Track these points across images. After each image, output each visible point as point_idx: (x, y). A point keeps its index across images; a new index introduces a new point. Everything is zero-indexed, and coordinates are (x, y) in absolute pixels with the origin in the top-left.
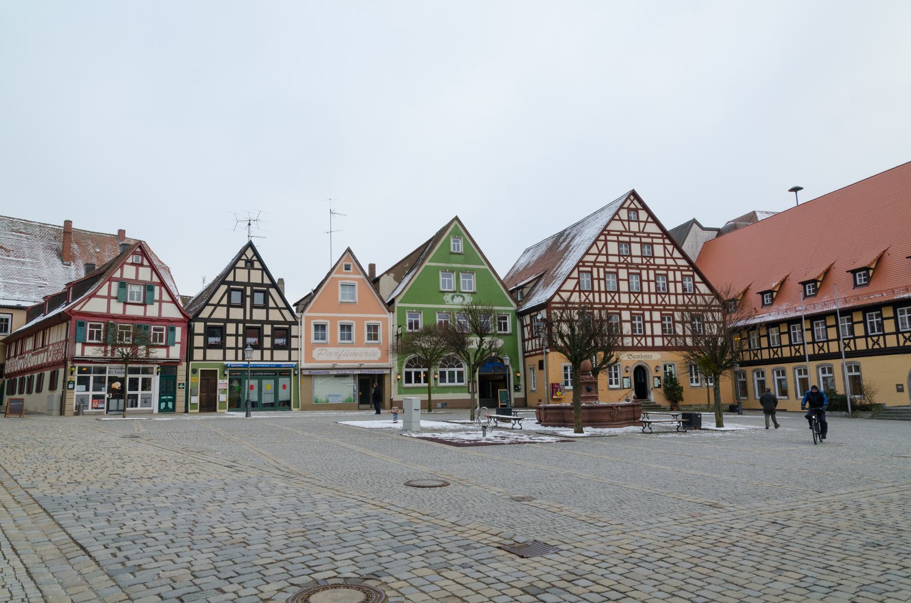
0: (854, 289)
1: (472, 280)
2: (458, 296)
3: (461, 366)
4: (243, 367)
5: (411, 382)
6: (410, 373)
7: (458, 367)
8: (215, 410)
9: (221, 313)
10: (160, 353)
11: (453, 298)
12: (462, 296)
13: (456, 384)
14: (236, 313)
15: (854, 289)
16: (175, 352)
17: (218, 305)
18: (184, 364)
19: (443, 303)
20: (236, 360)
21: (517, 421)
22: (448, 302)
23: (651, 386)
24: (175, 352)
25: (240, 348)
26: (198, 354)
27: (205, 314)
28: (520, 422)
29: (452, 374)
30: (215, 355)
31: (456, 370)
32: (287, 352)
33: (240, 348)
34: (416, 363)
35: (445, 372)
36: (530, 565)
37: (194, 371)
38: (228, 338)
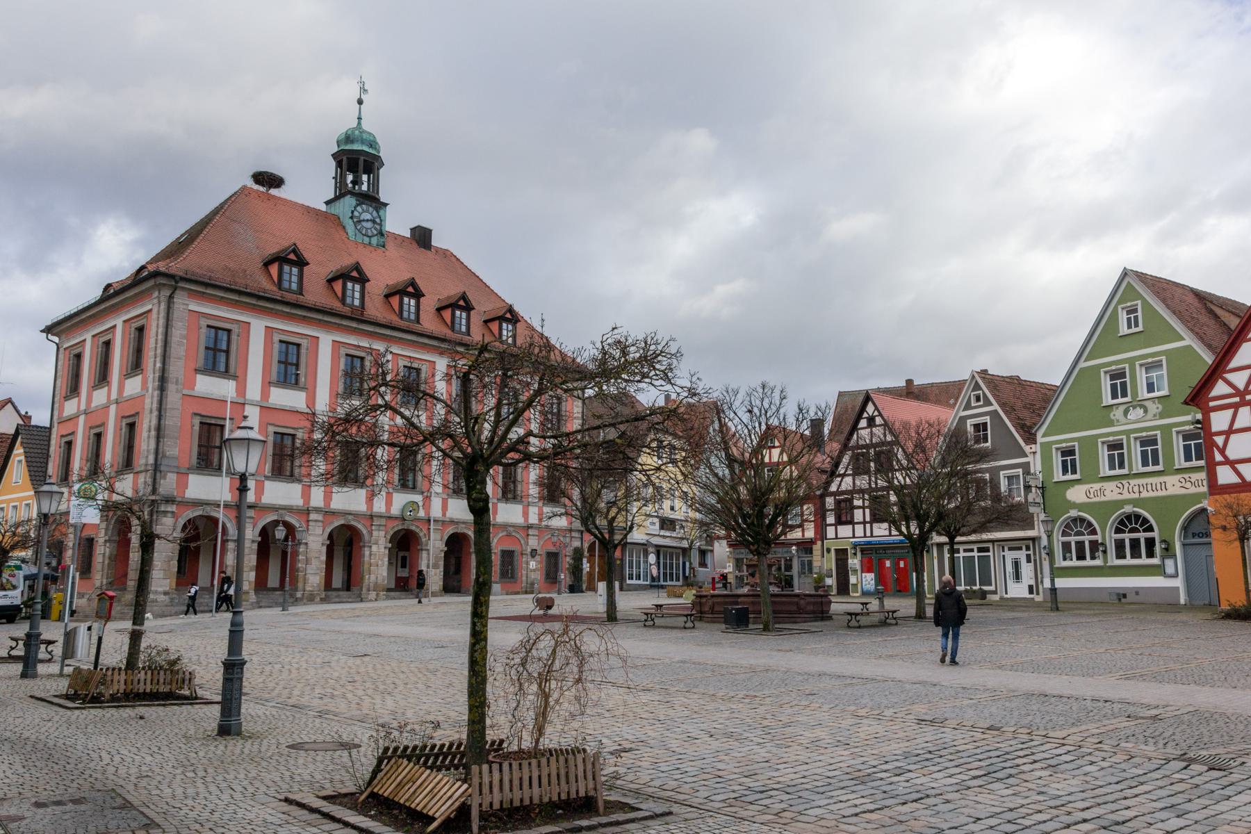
0: (41, 331)
1: (1154, 374)
2: (1134, 407)
3: (1150, 529)
4: (899, 543)
5: (1124, 557)
6: (1069, 543)
7: (1144, 531)
8: (848, 594)
9: (847, 483)
10: (797, 534)
11: (1126, 412)
12: (1141, 406)
13: (1075, 563)
14: (862, 482)
15: (41, 331)
16: (810, 534)
17: (843, 476)
18: (819, 543)
19: (1111, 423)
20: (865, 536)
21: (853, 616)
22: (1118, 421)
23: (98, 552)
24: (810, 534)
25: (868, 522)
26: (830, 532)
27: (833, 488)
28: (858, 618)
29: (1135, 544)
30: (845, 531)
31: (1142, 536)
32: (851, 526)
33: (868, 522)
34: (1127, 527)
35: (1083, 542)
36: (760, 802)
37: (829, 551)
38: (855, 511)
